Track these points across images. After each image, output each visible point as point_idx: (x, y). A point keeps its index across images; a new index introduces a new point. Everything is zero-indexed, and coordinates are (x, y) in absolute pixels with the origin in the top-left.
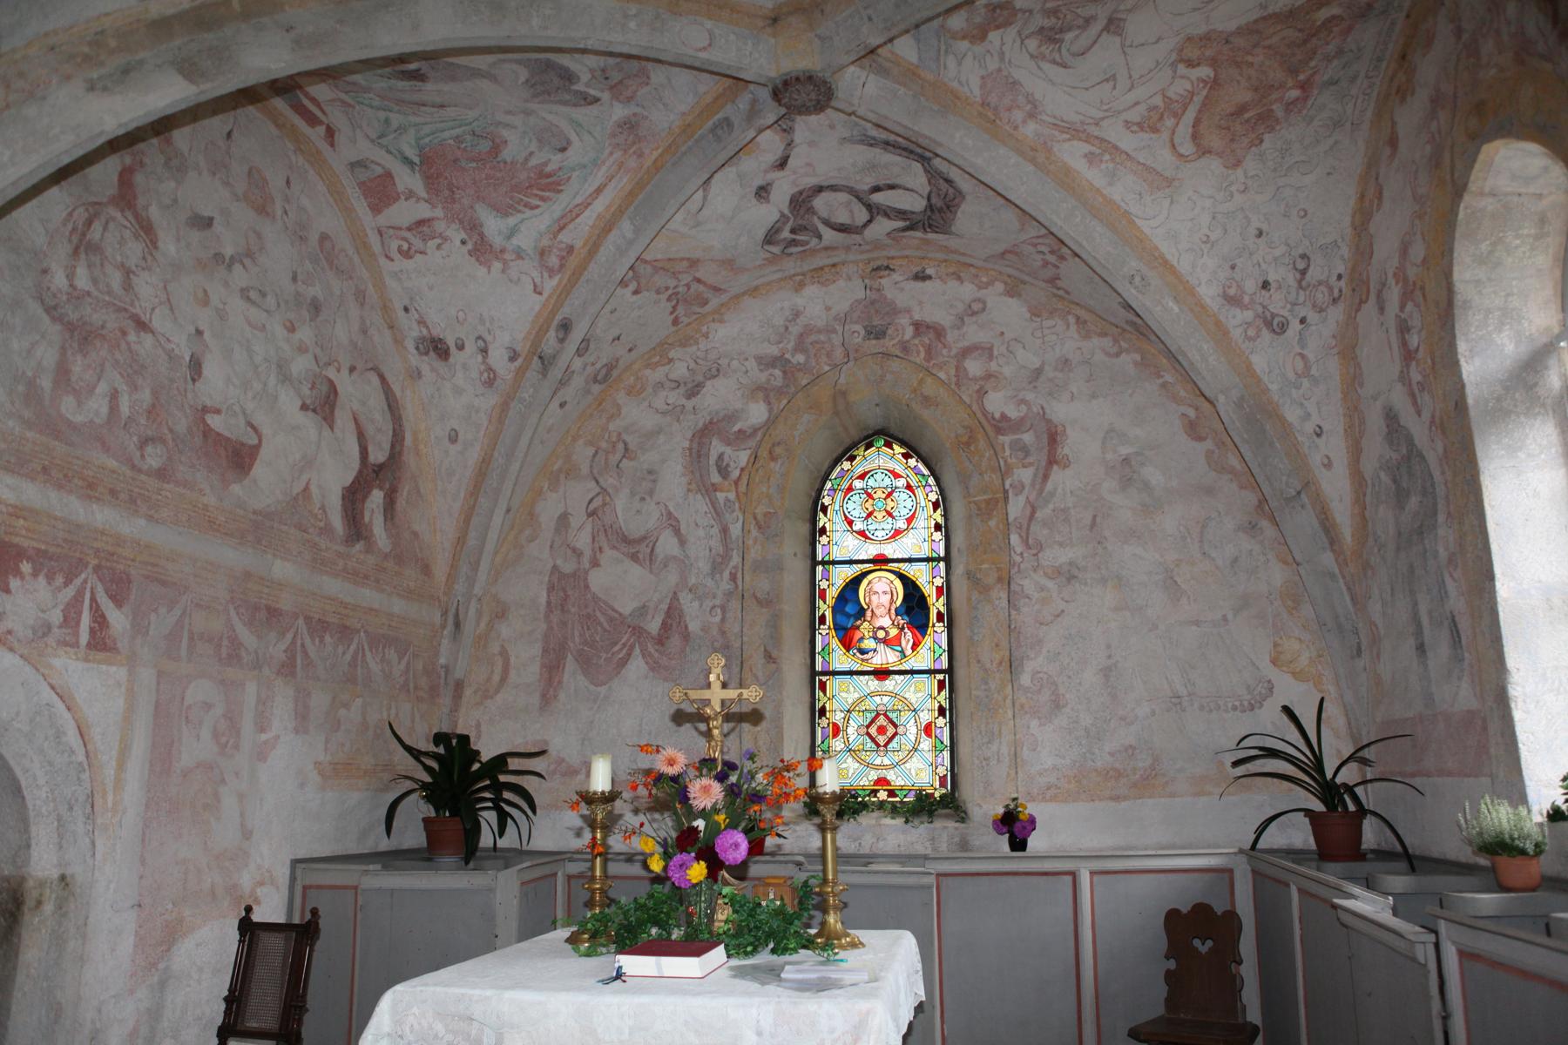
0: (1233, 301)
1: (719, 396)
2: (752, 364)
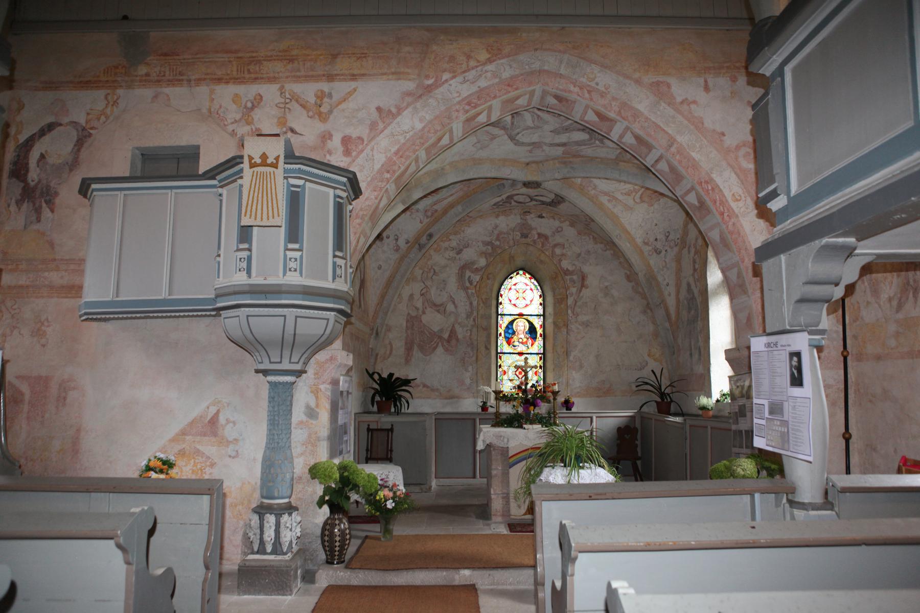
0: (646, 244)
1: (469, 254)
2: (480, 244)
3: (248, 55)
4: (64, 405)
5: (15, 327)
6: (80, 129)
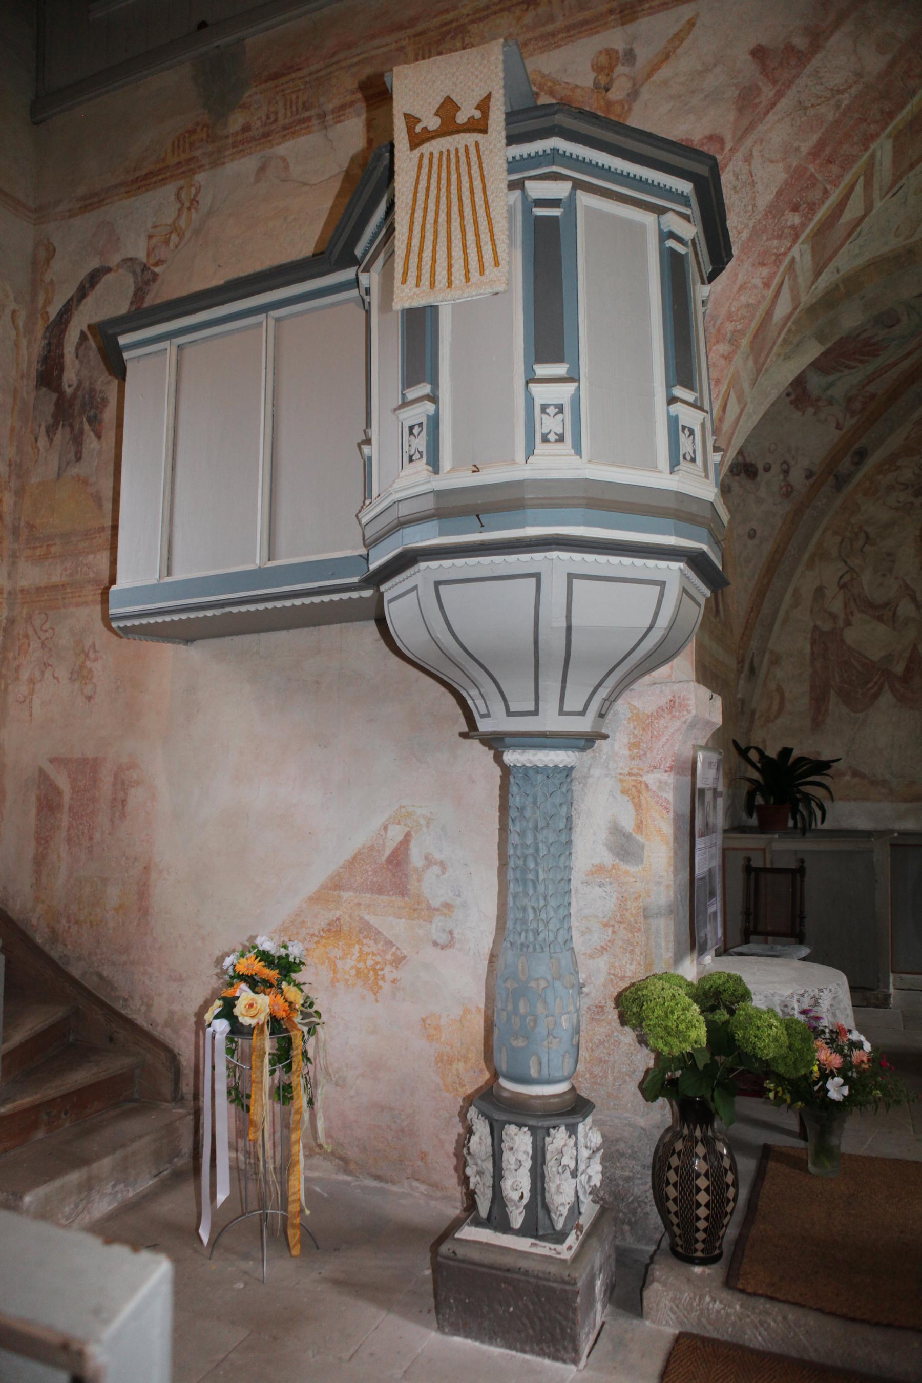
3: (437, 21)
4: (123, 815)
5: (46, 665)
6: (139, 270)
